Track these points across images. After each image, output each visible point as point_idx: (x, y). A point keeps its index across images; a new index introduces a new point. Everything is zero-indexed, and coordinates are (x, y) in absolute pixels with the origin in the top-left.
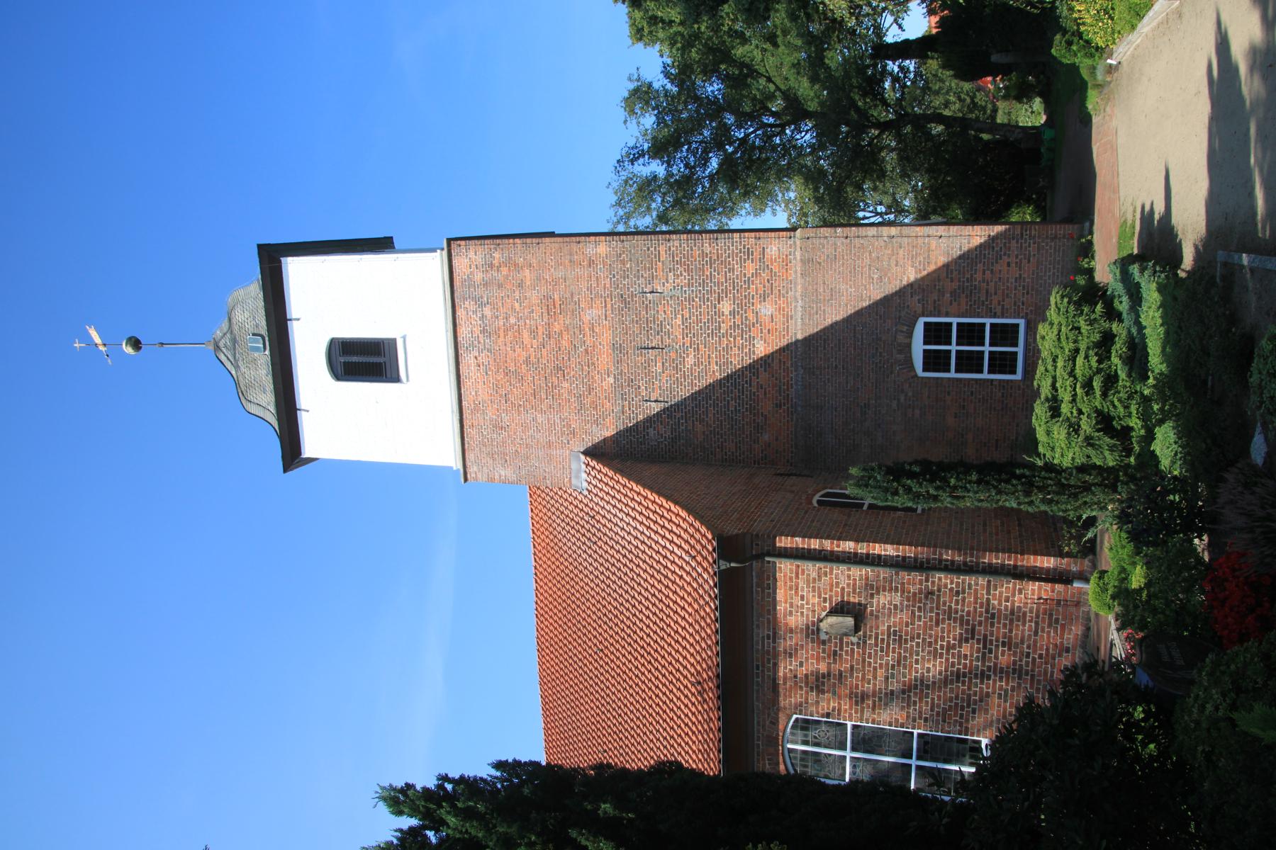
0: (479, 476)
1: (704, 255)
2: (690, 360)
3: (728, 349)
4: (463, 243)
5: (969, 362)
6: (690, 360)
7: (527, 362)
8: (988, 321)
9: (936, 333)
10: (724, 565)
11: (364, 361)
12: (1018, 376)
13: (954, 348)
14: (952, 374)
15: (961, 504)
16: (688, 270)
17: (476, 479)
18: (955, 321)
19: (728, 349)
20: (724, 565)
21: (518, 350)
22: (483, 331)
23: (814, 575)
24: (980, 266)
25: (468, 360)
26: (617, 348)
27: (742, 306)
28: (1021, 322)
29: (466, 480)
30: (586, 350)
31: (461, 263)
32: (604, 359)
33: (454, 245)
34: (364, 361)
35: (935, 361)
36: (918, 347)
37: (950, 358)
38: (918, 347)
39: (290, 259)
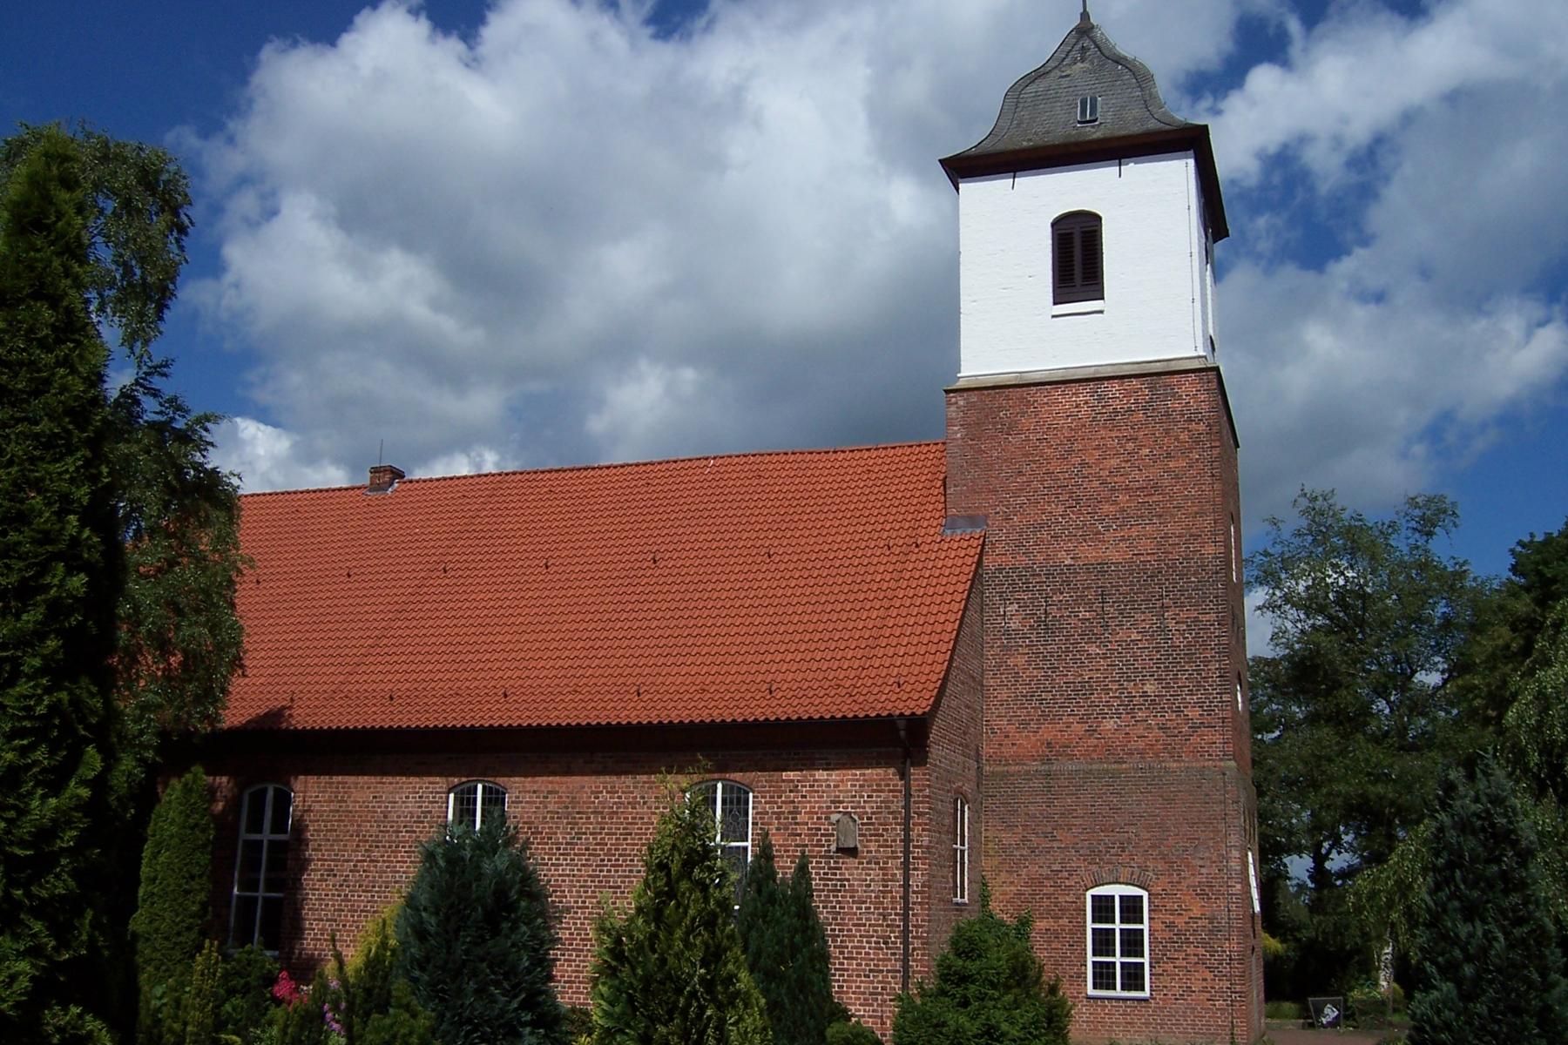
0: (953, 408)
1: (1206, 662)
2: (1093, 650)
3: (1107, 690)
4: (1214, 385)
5: (1103, 942)
6: (1093, 650)
7: (1083, 464)
8: (1146, 960)
9: (1132, 908)
10: (901, 724)
11: (1078, 258)
12: (1091, 991)
13: (1118, 959)
14: (1090, 926)
15: (38, 429)
16: (1189, 645)
17: (949, 404)
18: (1145, 926)
19: (1107, 690)
20: (901, 724)
21: (1096, 453)
22: (1115, 411)
23: (893, 807)
24: (1201, 951)
25: (1083, 395)
26: (1101, 568)
27: (1153, 703)
28: (1147, 993)
29: (947, 392)
30: (1099, 533)
31: (1187, 387)
32: (1089, 553)
33: (1212, 375)
34: (1078, 258)
35: (1103, 907)
36: (1117, 891)
37: (1107, 922)
38: (1117, 891)
39: (1191, 162)
